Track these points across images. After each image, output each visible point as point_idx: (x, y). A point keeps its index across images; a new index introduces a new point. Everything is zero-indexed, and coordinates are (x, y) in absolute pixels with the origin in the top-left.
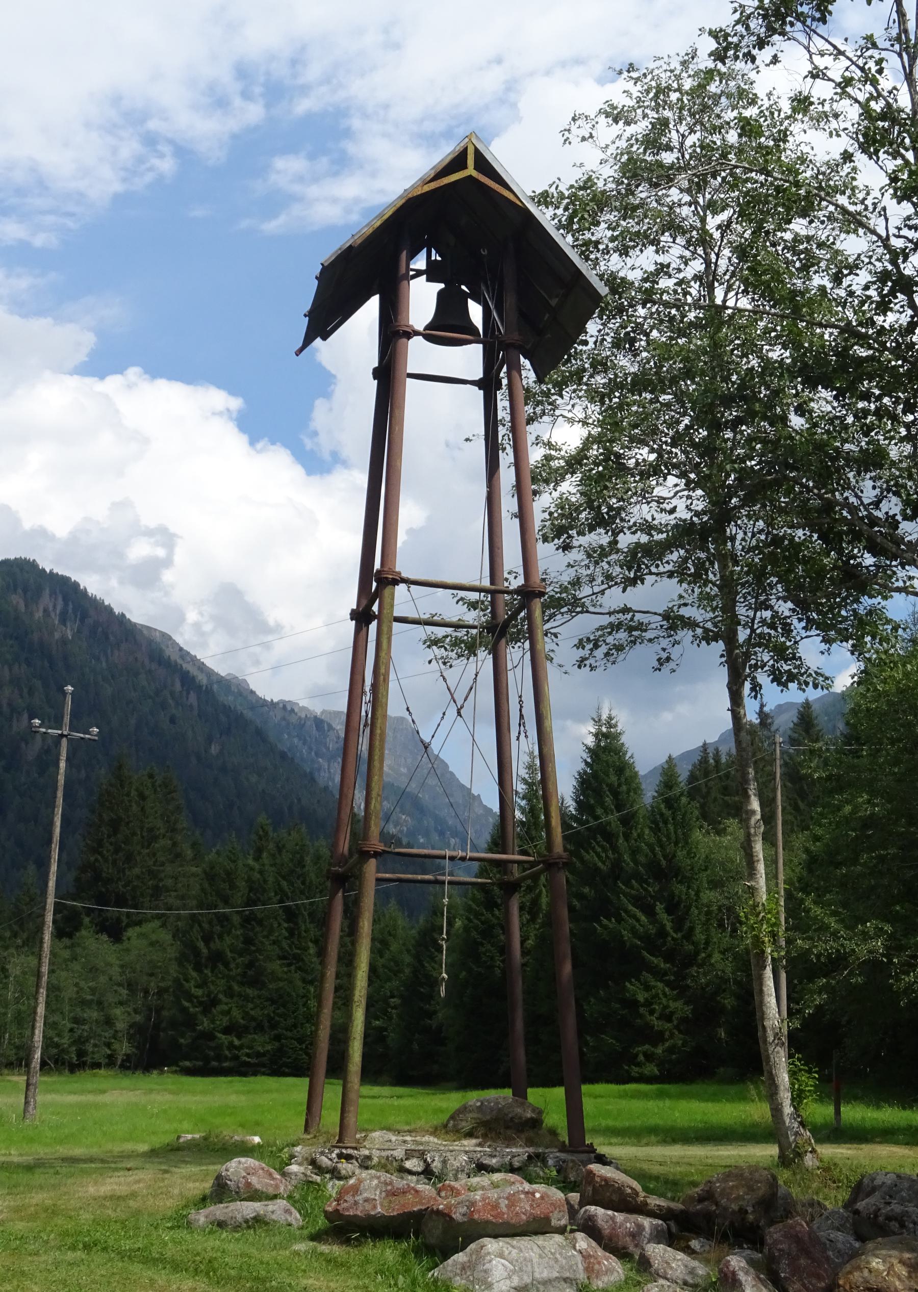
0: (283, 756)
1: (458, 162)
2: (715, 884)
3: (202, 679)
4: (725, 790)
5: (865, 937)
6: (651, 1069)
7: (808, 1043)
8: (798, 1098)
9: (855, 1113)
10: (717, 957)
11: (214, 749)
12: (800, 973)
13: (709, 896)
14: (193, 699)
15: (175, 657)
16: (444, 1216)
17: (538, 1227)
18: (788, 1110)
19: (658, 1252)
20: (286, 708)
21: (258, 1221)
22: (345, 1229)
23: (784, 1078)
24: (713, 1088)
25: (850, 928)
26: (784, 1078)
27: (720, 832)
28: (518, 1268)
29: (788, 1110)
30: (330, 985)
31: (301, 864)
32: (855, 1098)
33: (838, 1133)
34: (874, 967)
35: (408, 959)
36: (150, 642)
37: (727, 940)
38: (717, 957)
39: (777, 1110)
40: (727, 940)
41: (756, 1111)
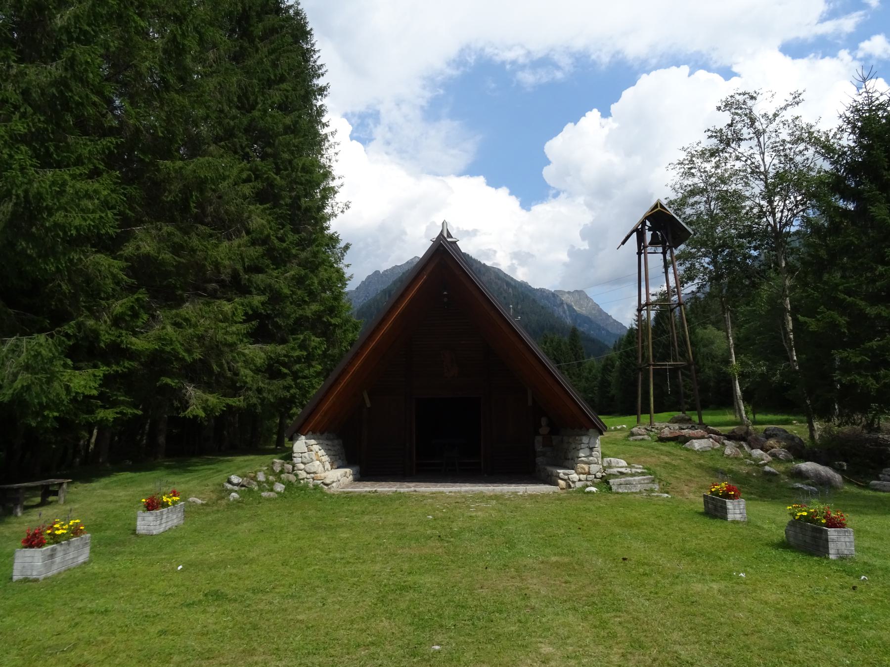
0: (543, 307)
1: (656, 206)
2: (705, 346)
3: (513, 283)
4: (704, 311)
5: (760, 366)
6: (687, 406)
7: (748, 397)
8: (746, 413)
9: (759, 417)
10: (707, 370)
11: (519, 307)
12: (743, 376)
13: (703, 350)
14: (511, 290)
15: (503, 276)
16: (684, 436)
17: (703, 437)
18: (744, 415)
19: (726, 442)
20: (542, 291)
21: (643, 439)
22: (662, 440)
23: (743, 408)
24: (710, 412)
25: (754, 364)
26: (743, 408)
27: (706, 328)
28: (700, 444)
29: (744, 415)
30: (358, 363)
31: (560, 345)
32: (760, 413)
33: (755, 423)
34: (762, 375)
35: (599, 375)
36: (494, 272)
37: (710, 364)
38: (707, 370)
39: (741, 416)
40: (710, 364)
41: (730, 417)
